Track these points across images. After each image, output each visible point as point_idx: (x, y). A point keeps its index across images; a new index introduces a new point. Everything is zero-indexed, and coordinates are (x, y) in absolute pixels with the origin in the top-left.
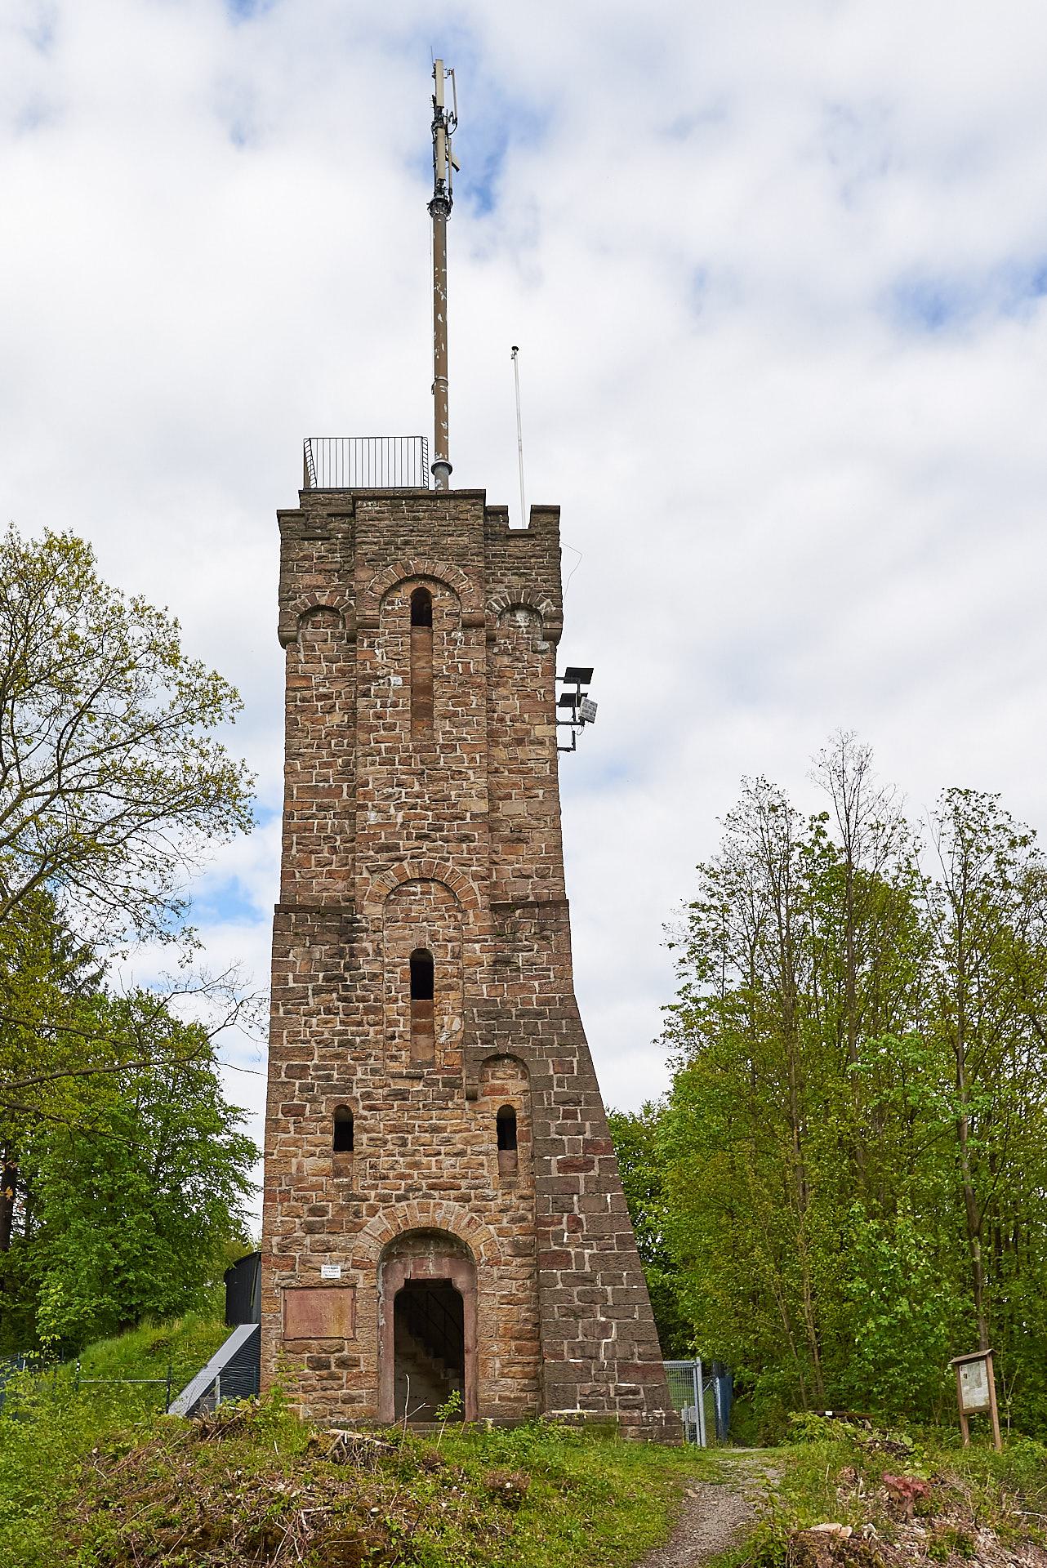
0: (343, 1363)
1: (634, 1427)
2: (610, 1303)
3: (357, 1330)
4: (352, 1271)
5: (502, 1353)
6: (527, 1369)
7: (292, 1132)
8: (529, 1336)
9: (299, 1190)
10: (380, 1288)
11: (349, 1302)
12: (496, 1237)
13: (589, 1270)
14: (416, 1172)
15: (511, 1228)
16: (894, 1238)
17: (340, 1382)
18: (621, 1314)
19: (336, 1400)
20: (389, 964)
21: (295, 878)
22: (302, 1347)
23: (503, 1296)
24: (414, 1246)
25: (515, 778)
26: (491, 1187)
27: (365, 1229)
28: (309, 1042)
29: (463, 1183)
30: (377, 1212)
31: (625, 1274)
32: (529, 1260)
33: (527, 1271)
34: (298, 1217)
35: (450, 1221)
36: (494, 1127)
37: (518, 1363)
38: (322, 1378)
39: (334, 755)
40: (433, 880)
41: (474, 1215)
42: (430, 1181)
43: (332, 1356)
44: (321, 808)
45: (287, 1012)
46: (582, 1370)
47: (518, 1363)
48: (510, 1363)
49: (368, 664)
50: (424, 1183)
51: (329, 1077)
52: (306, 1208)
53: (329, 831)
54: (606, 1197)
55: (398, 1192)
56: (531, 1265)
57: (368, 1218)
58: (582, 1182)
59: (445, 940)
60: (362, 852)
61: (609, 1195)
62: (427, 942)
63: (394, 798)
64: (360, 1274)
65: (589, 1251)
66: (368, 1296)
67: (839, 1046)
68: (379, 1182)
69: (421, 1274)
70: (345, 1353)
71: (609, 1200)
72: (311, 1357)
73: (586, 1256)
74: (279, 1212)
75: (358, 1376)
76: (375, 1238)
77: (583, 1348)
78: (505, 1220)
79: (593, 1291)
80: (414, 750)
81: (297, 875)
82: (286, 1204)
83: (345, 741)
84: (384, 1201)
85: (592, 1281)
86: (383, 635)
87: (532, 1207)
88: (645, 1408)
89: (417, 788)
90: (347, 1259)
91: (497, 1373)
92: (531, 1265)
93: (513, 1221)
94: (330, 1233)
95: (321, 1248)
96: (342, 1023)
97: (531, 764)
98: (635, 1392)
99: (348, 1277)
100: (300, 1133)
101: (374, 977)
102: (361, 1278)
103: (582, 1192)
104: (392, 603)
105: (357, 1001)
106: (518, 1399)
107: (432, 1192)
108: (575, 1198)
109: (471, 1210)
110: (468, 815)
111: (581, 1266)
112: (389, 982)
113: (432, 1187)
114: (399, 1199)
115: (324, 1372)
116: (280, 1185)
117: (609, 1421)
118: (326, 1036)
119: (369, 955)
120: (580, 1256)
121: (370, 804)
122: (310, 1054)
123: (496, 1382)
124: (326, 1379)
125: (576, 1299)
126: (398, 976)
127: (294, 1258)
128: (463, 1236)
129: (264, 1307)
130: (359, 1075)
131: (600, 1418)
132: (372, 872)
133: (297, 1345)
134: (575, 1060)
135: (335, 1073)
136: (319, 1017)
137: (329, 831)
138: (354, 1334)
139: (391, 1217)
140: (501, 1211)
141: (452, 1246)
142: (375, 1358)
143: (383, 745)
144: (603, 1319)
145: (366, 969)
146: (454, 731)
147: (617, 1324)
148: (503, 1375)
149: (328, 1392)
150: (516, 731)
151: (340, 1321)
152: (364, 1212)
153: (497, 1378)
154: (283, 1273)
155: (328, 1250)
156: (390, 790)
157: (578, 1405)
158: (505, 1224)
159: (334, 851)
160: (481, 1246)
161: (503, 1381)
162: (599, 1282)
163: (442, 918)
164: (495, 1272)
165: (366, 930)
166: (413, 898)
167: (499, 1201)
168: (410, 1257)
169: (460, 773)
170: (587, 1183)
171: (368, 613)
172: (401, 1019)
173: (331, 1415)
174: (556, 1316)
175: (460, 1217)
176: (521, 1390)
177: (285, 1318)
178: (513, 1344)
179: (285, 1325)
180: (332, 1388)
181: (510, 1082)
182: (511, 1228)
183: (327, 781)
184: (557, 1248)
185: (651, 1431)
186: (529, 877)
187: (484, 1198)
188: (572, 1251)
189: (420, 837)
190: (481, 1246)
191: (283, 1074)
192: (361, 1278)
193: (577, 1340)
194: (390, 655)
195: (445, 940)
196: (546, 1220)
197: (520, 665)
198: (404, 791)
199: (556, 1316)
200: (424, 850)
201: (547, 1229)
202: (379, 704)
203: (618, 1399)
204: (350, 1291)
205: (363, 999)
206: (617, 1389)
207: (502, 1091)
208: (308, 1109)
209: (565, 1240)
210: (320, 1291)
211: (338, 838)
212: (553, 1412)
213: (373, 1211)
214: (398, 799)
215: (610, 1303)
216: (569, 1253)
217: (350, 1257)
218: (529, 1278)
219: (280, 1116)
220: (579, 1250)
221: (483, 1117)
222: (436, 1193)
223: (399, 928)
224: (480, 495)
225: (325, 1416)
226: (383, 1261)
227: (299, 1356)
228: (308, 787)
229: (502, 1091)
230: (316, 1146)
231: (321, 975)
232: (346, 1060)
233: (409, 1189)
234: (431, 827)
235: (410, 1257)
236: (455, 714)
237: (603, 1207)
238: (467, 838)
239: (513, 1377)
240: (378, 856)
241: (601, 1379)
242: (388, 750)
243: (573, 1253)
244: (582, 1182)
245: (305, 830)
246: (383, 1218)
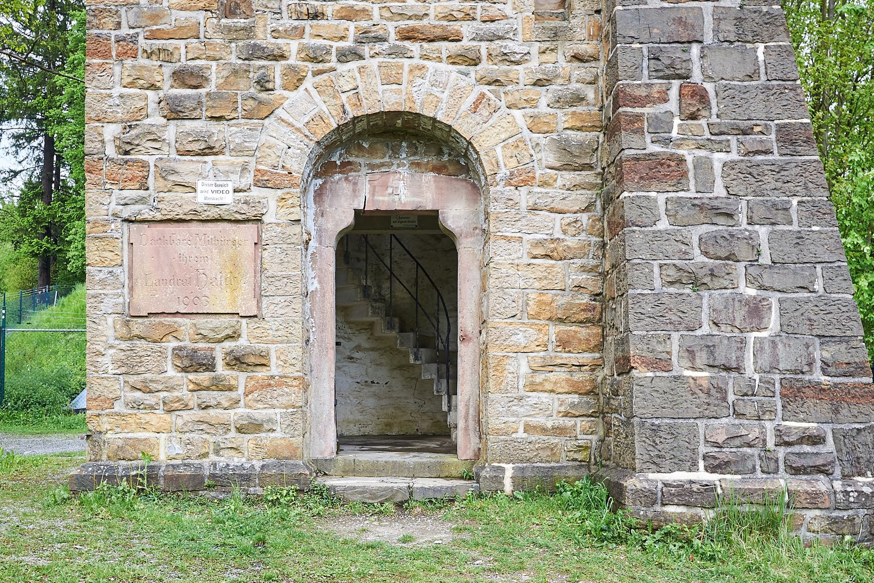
0: (237, 361)
1: (818, 512)
2: (765, 260)
3: (265, 301)
4: (256, 193)
5: (533, 347)
6: (578, 376)
8: (582, 316)
9: (152, 36)
10: (311, 226)
11: (249, 248)
12: (526, 132)
13: (724, 193)
14: (376, 7)
15: (555, 116)
17: (233, 395)
18: (789, 281)
19: (226, 427)
22: (162, 331)
23: (539, 243)
24: (371, 152)
26: (520, 37)
27: (279, 112)
29: (466, 29)
30: (301, 80)
31: (795, 201)
32: (588, 176)
33: (581, 198)
34: (153, 87)
35: (439, 101)
37: (561, 365)
38: (199, 388)
41: (485, 89)
42: (404, 24)
43: (218, 347)
46: (708, 394)
47: (561, 365)
48: (550, 366)
50: (391, 27)
52: (168, 70)
54: (755, 50)
55: (342, 44)
56: (592, 186)
57: (286, 93)
58: (709, 21)
61: (761, 47)
64: (271, 197)
65: (722, 156)
66: (285, 239)
67: (766, 24)
68: (307, 24)
69: (384, 202)
70: (243, 342)
71: (761, 57)
72: (180, 349)
73: (717, 167)
74: (117, 78)
75: (267, 385)
76: (298, 130)
77: (711, 349)
78: (544, 102)
79: (732, 236)
82: (129, 62)
84: (314, 60)
85: (730, 216)
87: (596, 77)
88: (838, 472)
90: (244, 169)
91: (522, 383)
92: (592, 186)
93: (559, 102)
94: (212, 118)
95: (196, 147)
98: (816, 440)
99: (246, 202)
102: (272, 205)
103: (709, 38)
106: (559, 431)
107: (407, 44)
109: (480, 80)
111: (707, 184)
113: (408, 36)
114: (344, 56)
115: (204, 377)
116: (118, 25)
117: (767, 499)
123: (521, 399)
124: (208, 389)
125: (697, 251)
127: (145, 165)
128: (465, 127)
129: (91, 256)
131: (752, 492)
133: (153, 326)
138: (259, 308)
139: (330, 91)
140: (538, 83)
141: (440, 153)
142: (297, 352)
144: (752, 292)
147: (780, 301)
148: (533, 387)
149: (211, 412)
151: (233, 279)
152: (278, 81)
153: (522, 393)
154: (126, 193)
155: (209, 151)
157: (701, 464)
158: (543, 107)
160: (499, 149)
161: (534, 397)
162: (743, 218)
164: (524, 198)
167: (534, 64)
168: (364, 170)
170: (718, 20)
173: (217, 452)
174: (657, 283)
175: (458, 94)
176: (566, 415)
177: (131, 277)
178: (554, 330)
179: (131, 289)
180: (218, 405)
182: (555, 116)
185: (851, 520)
187: (506, 58)
188: (689, 155)
190: (499, 149)
192: (272, 205)
193: (699, 333)
196: (638, 92)
199: (657, 283)
201: (638, 110)
203: (782, 452)
204: (251, 228)
206: (779, 432)
209: (674, 134)
210: (195, 227)
212: (651, 476)
213: (295, 80)
215: (765, 260)
216: (681, 160)
217: (252, 166)
218: (587, 209)
220: (702, 153)
222: (414, 47)
225: (205, 455)
226: (316, 176)
227: (156, 346)
233: (366, 37)
235: (364, 170)
237: (749, 70)
239: (552, 391)
241: (750, 410)
243: (689, 159)
244: (709, 21)
246: (314, 92)
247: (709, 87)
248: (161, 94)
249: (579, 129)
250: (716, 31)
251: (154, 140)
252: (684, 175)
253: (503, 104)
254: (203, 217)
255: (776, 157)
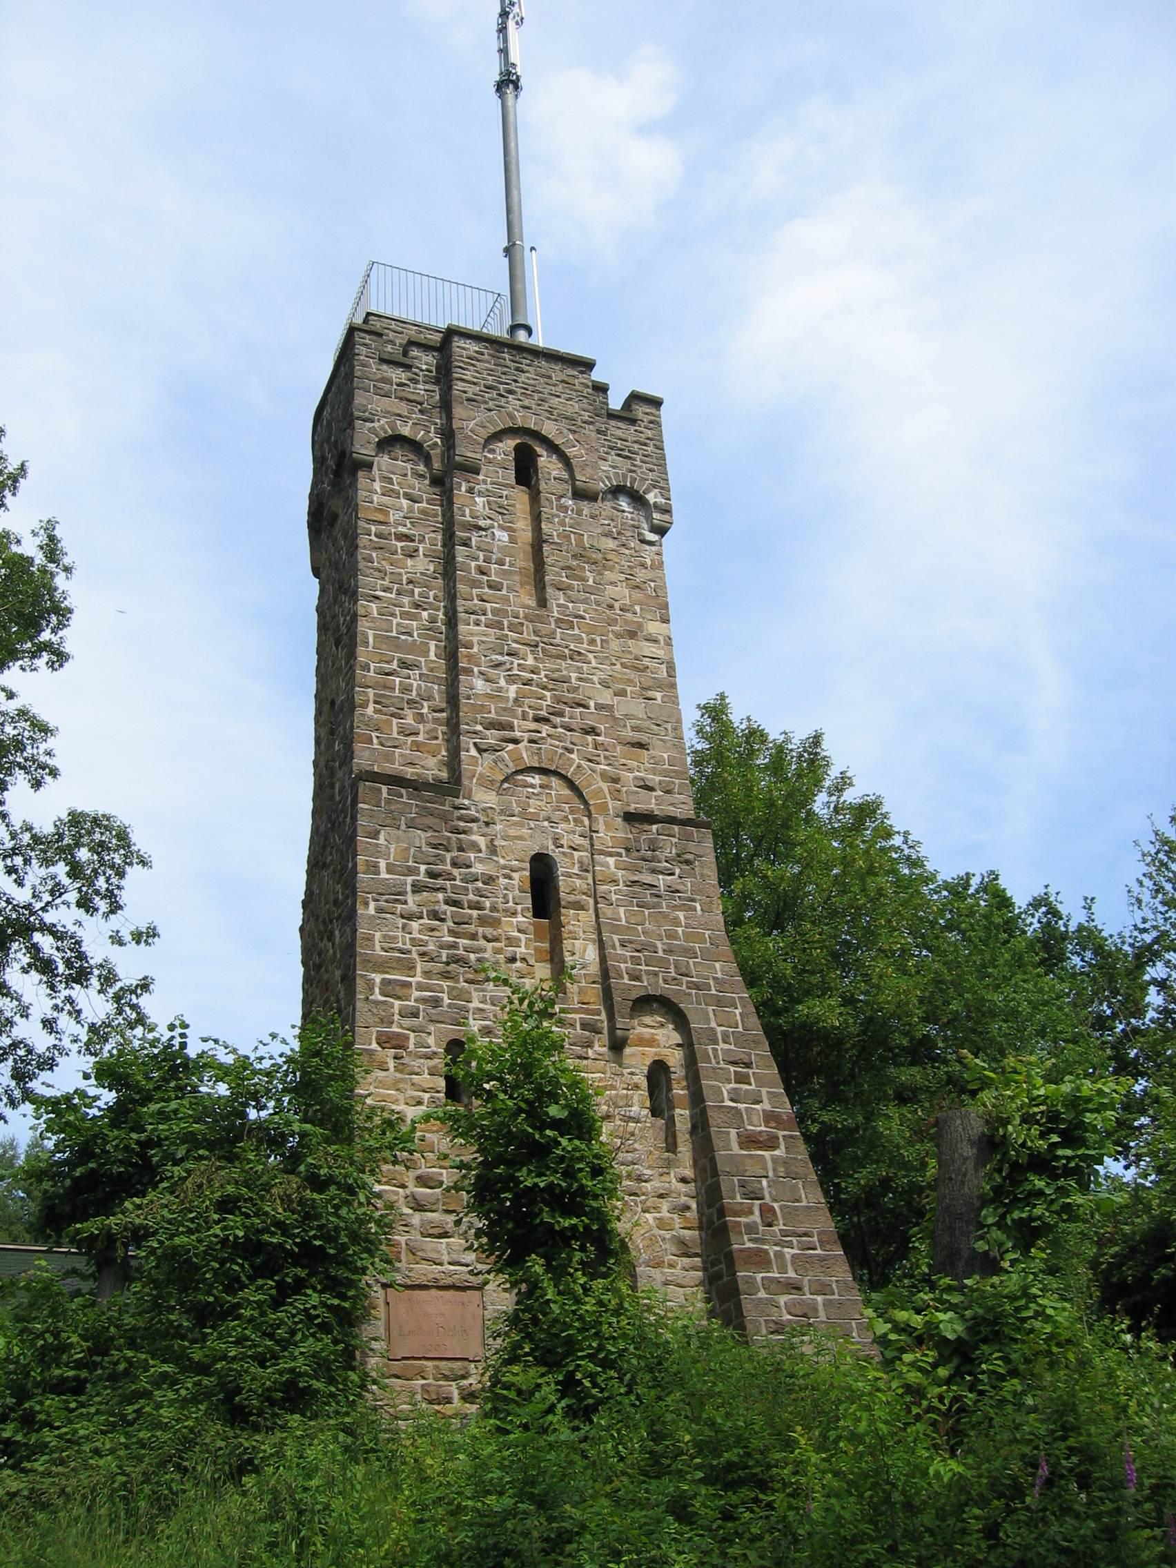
7: (392, 1069)
16: (273, 1403)
20: (504, 867)
21: (372, 743)
25: (632, 675)
28: (409, 952)
34: (403, 1186)
36: (645, 1084)
39: (417, 606)
40: (556, 773)
44: (404, 664)
45: (380, 910)
49: (467, 511)
51: (436, 1002)
53: (414, 693)
59: (571, 847)
60: (467, 724)
62: (551, 850)
63: (504, 667)
80: (526, 617)
81: (375, 741)
83: (431, 593)
86: (485, 479)
89: (530, 661)
95: (435, 1231)
96: (452, 932)
97: (646, 662)
100: (401, 1072)
101: (489, 880)
104: (492, 451)
105: (470, 908)
108: (764, 1182)
110: (592, 704)
112: (506, 889)
118: (431, 947)
119: (480, 851)
120: (779, 1255)
121: (476, 669)
122: (411, 968)
126: (516, 882)
130: (475, 1004)
132: (480, 750)
134: (737, 1012)
135: (445, 996)
136: (421, 921)
137: (414, 693)
140: (661, 1196)
143: (488, 605)
145: (478, 869)
146: (570, 605)
150: (627, 622)
156: (500, 658)
158: (665, 1213)
159: (420, 718)
163: (566, 819)
165: (475, 820)
166: (530, 790)
169: (579, 653)
171: (469, 454)
172: (522, 936)
181: (660, 1031)
183: (410, 634)
184: (751, 1245)
186: (651, 789)
188: (772, 1250)
189: (537, 719)
191: (377, 990)
194: (494, 506)
195: (571, 847)
197: (627, 552)
198: (516, 662)
199: (764, 1332)
200: (544, 735)
202: (482, 558)
205: (477, 906)
207: (651, 1042)
208: (412, 1041)
210: (434, 1292)
211: (425, 704)
214: (509, 670)
219: (374, 1046)
221: (632, 1074)
223: (515, 824)
224: (588, 365)
228: (388, 637)
229: (651, 1042)
230: (424, 1091)
231: (423, 868)
232: (457, 982)
234: (552, 710)
236: (570, 587)
238: (592, 731)
240: (488, 732)
242: (495, 612)
245: (385, 687)
247: (776, 1205)
248: (408, 1191)
249: (689, 1229)
250: (774, 1170)
251: (406, 1225)
252: (770, 1262)
253: (639, 1209)
254: (441, 1283)
255: (819, 1252)
